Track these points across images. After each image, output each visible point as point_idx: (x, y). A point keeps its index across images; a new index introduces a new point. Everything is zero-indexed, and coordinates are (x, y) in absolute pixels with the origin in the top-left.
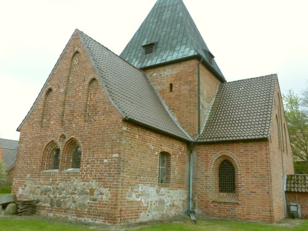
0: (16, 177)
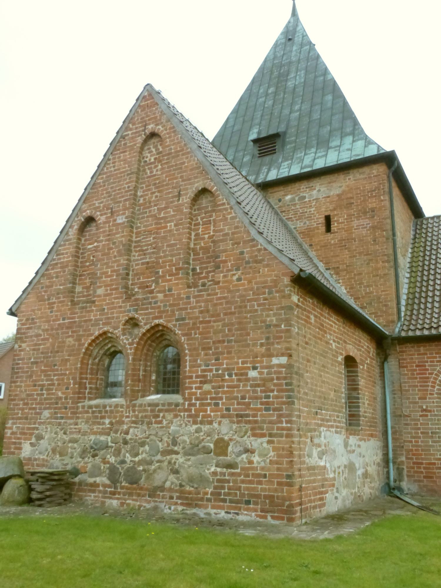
0: (13, 419)
